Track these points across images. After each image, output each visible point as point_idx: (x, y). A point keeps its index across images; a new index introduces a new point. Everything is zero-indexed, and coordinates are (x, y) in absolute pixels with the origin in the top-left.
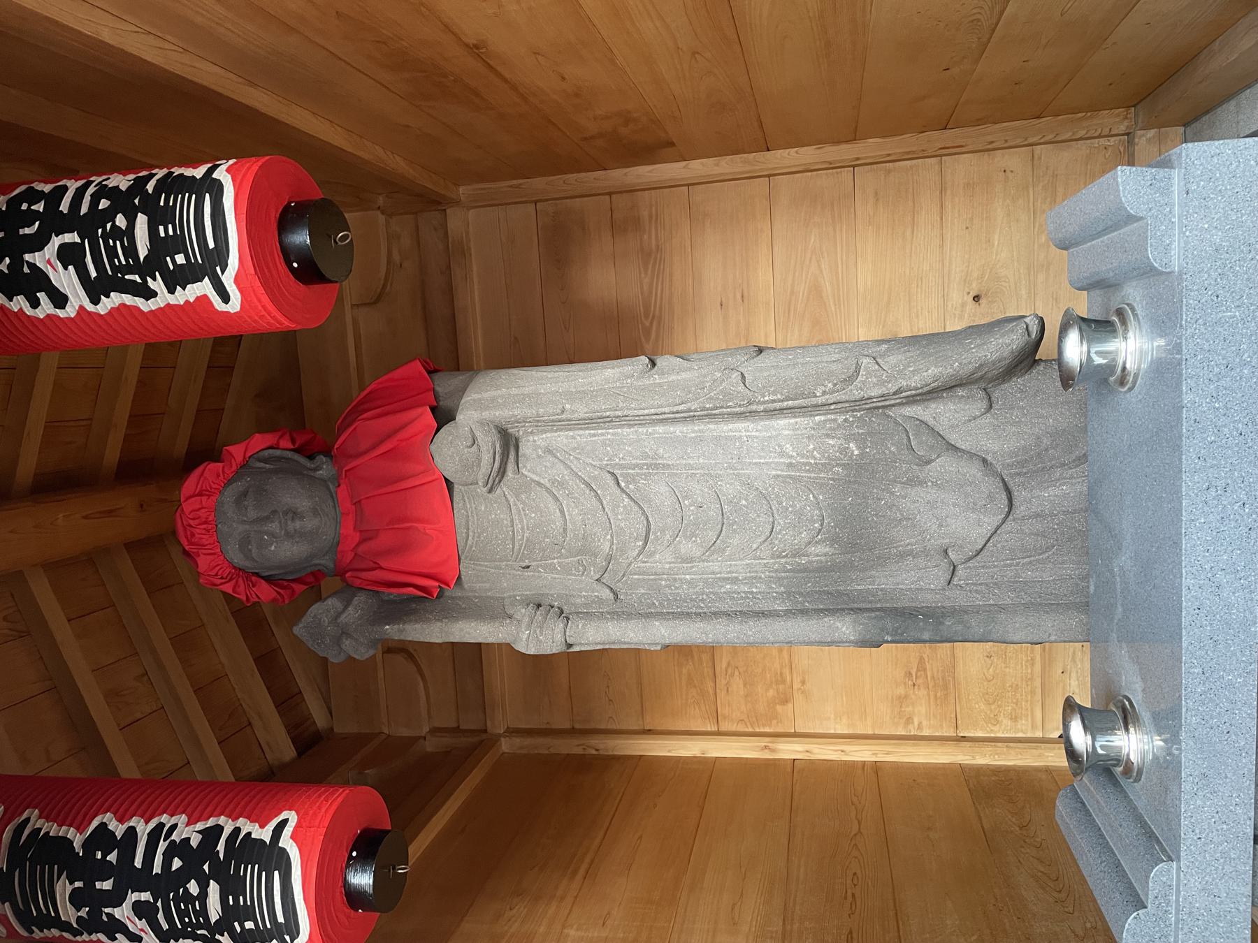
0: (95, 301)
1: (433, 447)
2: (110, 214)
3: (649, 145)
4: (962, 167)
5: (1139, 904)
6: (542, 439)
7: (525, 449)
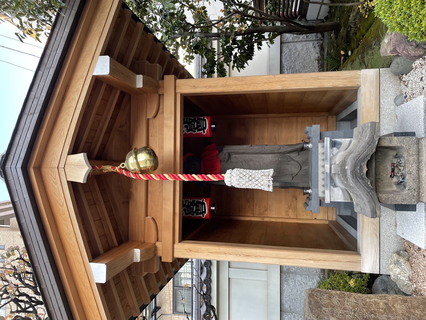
2: (192, 122)
4: (300, 119)
5: (308, 205)
6: (234, 156)
7: (232, 157)
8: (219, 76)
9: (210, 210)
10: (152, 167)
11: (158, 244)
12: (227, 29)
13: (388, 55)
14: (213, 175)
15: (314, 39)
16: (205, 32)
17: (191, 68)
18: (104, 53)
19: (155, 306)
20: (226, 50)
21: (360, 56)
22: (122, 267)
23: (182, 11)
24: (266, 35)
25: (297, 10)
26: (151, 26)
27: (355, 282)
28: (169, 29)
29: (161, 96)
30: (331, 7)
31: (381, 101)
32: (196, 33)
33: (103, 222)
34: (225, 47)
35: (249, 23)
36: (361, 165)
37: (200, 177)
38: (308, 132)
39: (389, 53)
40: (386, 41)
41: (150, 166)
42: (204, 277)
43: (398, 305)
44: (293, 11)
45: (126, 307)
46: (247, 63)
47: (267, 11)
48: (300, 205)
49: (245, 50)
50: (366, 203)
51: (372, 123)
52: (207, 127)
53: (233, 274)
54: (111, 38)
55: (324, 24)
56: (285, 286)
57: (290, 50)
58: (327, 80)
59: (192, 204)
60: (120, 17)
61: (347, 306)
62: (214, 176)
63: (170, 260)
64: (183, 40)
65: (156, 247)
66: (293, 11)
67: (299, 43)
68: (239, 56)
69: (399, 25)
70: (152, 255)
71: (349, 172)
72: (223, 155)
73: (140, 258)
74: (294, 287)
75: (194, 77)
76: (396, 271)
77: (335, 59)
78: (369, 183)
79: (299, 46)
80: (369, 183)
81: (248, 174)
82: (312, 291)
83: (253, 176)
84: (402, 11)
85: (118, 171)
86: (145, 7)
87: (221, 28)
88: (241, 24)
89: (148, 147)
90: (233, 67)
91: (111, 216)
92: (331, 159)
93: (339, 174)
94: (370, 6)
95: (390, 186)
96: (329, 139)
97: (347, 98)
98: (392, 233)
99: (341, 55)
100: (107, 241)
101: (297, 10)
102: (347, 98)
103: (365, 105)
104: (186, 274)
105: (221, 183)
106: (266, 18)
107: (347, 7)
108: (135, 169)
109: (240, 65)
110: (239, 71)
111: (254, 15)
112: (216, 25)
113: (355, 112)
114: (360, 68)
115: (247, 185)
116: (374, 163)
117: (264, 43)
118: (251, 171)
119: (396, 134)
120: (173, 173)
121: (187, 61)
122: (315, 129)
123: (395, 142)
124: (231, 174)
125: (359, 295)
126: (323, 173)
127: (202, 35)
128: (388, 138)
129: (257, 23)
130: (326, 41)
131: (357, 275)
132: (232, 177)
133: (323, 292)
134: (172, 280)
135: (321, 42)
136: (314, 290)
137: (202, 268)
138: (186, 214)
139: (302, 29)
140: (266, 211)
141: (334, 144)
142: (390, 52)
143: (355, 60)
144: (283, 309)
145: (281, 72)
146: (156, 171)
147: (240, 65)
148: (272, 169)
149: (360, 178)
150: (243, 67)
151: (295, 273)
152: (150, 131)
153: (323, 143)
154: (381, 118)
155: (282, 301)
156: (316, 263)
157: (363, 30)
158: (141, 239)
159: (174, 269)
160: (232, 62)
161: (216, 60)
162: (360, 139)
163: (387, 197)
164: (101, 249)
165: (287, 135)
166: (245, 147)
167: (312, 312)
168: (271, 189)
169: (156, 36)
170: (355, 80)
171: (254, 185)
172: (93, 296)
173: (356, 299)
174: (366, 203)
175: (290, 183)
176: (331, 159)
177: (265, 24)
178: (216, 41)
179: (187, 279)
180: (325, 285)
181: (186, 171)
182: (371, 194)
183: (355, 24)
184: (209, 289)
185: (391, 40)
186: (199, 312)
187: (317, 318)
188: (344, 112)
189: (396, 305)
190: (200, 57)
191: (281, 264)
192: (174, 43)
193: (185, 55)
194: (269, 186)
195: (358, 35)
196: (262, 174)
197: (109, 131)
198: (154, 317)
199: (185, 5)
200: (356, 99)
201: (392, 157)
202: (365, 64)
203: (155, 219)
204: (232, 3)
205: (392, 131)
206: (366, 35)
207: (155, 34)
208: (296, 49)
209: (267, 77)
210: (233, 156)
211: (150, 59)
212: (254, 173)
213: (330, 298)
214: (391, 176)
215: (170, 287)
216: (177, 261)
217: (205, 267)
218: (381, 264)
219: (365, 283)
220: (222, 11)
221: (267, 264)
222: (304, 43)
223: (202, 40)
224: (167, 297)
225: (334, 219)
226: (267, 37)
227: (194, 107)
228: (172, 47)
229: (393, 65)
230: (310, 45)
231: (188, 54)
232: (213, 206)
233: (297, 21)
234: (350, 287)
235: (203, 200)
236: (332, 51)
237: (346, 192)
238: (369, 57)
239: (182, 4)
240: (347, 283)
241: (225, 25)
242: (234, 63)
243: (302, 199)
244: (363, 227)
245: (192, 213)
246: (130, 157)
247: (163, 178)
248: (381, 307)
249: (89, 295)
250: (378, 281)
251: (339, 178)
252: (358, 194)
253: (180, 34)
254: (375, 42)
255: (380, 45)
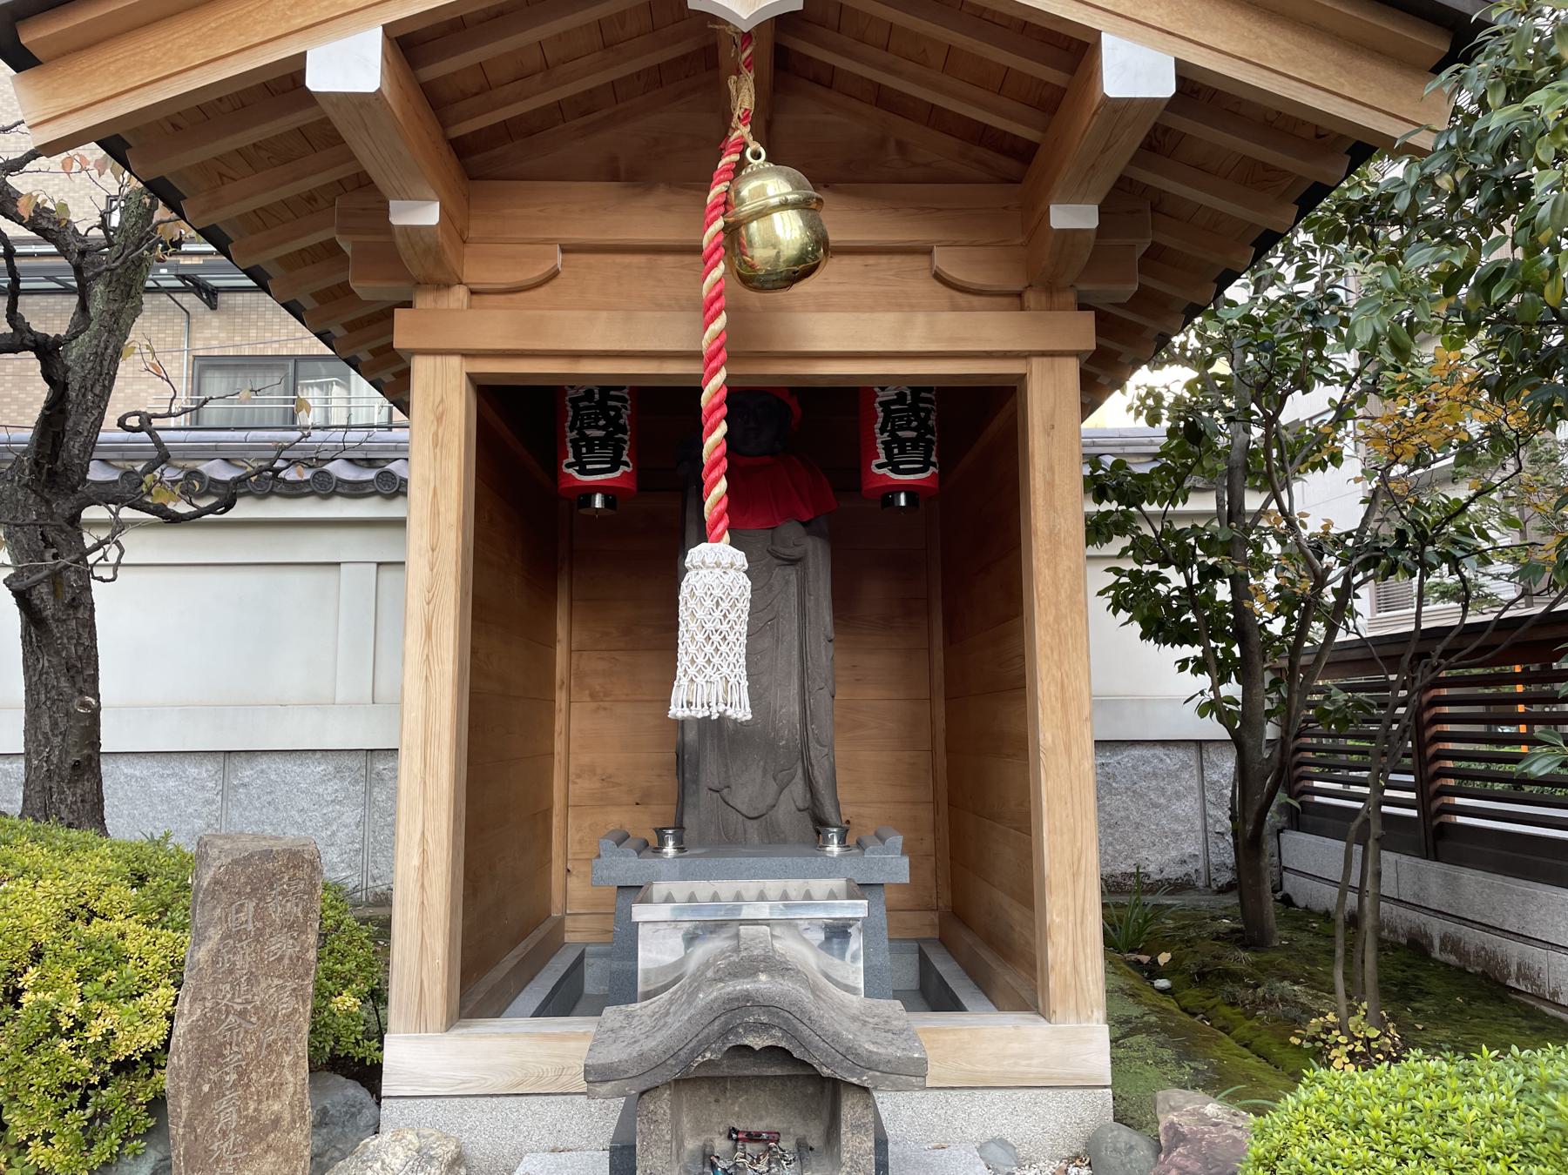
0: (881, 404)
1: (794, 523)
2: (918, 418)
3: (953, 636)
6: (793, 578)
8: (1088, 516)
9: (592, 490)
10: (752, 266)
11: (459, 295)
12: (1258, 548)
13: (1160, 1117)
14: (725, 500)
15: (1213, 859)
16: (1247, 464)
17: (1116, 416)
18: (1186, 75)
19: (218, 290)
20: (1182, 544)
21: (1153, 1019)
22: (371, 154)
23: (1327, 375)
24: (1232, 689)
25: (1318, 799)
26: (1274, 261)
27: (349, 1014)
28: (1264, 330)
29: (1016, 301)
30: (1327, 916)
31: (998, 1093)
32: (1248, 432)
33: (538, 77)
34: (1192, 541)
35: (1277, 627)
36: (773, 1027)
37: (717, 454)
38: (883, 840)
39: (1165, 1118)
40: (1212, 1108)
41: (756, 262)
42: (340, 470)
43: (274, 1163)
44: (1317, 784)
45: (218, 174)
46: (1131, 620)
47: (1320, 691)
48: (618, 818)
49: (1180, 611)
50: (637, 1047)
51: (923, 1062)
52: (899, 475)
53: (356, 582)
54: (1239, 101)
55: (1269, 893)
56: (318, 768)
57: (1173, 775)
58: (1071, 903)
59: (613, 422)
60: (1318, 136)
61: (264, 985)
62: (723, 505)
63: (400, 341)
64: (1219, 383)
65: (448, 286)
66: (1317, 784)
67: (1197, 806)
68: (1157, 591)
69: (1275, 1154)
70: (416, 271)
71: (745, 985)
72: (792, 534)
73: (405, 227)
74: (315, 798)
75: (1084, 425)
76: (394, 1154)
77: (1140, 933)
78: (708, 1055)
79: (1188, 806)
80: (708, 1055)
81: (732, 628)
82: (312, 863)
83: (724, 648)
84: (1329, 1165)
85: (736, 134)
86: (1351, 235)
87: (1264, 523)
88: (1274, 595)
89: (825, 252)
90: (1118, 571)
91: (558, 112)
92: (790, 923)
93: (737, 950)
94: (1334, 1053)
95: (698, 1130)
96: (862, 913)
97: (1006, 977)
98: (528, 1136)
99: (1154, 954)
100: (465, 96)
101: (1318, 799)
102: (1006, 977)
103: (980, 1037)
104: (348, 404)
105: (691, 530)
106: (1297, 687)
107: (1330, 975)
108: (742, 202)
109: (1125, 596)
110: (1100, 593)
111: (1307, 644)
112: (1273, 506)
113: (955, 1005)
114: (1114, 1020)
115: (693, 626)
116: (779, 1072)
117: (1205, 681)
118: (743, 639)
119: (881, 1144)
120: (733, 349)
121: (1140, 398)
122: (893, 864)
123: (855, 1143)
124: (732, 565)
125: (306, 1028)
126: (738, 897)
127: (1236, 455)
128: (871, 1118)
129: (1276, 655)
130: (1204, 902)
131: (374, 1018)
132: (718, 571)
133: (311, 900)
134: (322, 349)
135: (1200, 884)
136: (315, 869)
137: (370, 463)
138: (574, 401)
139: (1251, 817)
140: (593, 697)
141: (837, 932)
142: (1172, 1124)
143: (1139, 1003)
144: (236, 760)
145: (1099, 744)
146: (735, 285)
147: (1125, 596)
148: (749, 717)
149: (727, 1023)
150: (1116, 606)
151: (368, 802)
152: (884, 260)
153: (844, 893)
154: (936, 1092)
155: (265, 758)
156: (413, 875)
157: (1243, 1030)
158: (476, 229)
159: (365, 356)
160: (1136, 567)
161: (1145, 506)
162: (865, 1023)
163: (659, 1117)
164: (432, 71)
165: (869, 765)
166: (827, 617)
167: (235, 862)
168: (676, 711)
169: (1238, 282)
170: (1072, 1003)
171: (692, 649)
172: (257, 40)
173: (289, 1016)
174: (637, 1047)
175: (696, 781)
176: (790, 923)
177: (1273, 683)
178: (1213, 507)
179: (327, 410)
180: (332, 907)
181: (739, 399)
182: (672, 1062)
183: (1267, 1002)
184: (295, 491)
185: (1216, 1125)
186: (210, 452)
187: (216, 883)
188: (954, 966)
189: (271, 1157)
190: (1157, 450)
191: (403, 753)
192: (1209, 351)
193: (1164, 391)
194: (689, 704)
195: (1226, 1011)
196: (732, 681)
197: (882, 98)
198: (178, 283)
199: (1349, 387)
200: (1000, 1009)
201: (801, 1132)
202: (1124, 1037)
203: (554, 282)
204: (1355, 562)
205: (891, 1131)
206: (1227, 1039)
207: (1246, 278)
208: (1178, 796)
209: (1086, 694)
210: (792, 574)
211: (1155, 255)
212: (736, 649)
213: (291, 927)
214: (734, 1130)
215: (291, 345)
216: (401, 367)
217: (377, 477)
218: (418, 1101)
219: (347, 1047)
220: (1328, 525)
221: (399, 703)
222: (1198, 824)
223: (1218, 455)
224: (253, 333)
225: (568, 938)
226: (1224, 690)
227: (973, 424)
228: (1194, 343)
229: (1124, 1135)
230: (1192, 847)
231: (1166, 404)
232: (606, 501)
233: (1281, 797)
234: (331, 994)
235: (626, 464)
236: (1170, 923)
237: (672, 977)
238: (1149, 1052)
239: (1355, 379)
240: (345, 987)
241: (1271, 539)
242: (1132, 574)
243: (641, 823)
244: (546, 1036)
245: (580, 424)
246: (789, 181)
247: (713, 310)
248: (264, 1106)
249: (258, 28)
250: (355, 1091)
251: (722, 952)
252: (669, 1020)
253: (1242, 372)
254: (1202, 1072)
255: (1193, 1088)
